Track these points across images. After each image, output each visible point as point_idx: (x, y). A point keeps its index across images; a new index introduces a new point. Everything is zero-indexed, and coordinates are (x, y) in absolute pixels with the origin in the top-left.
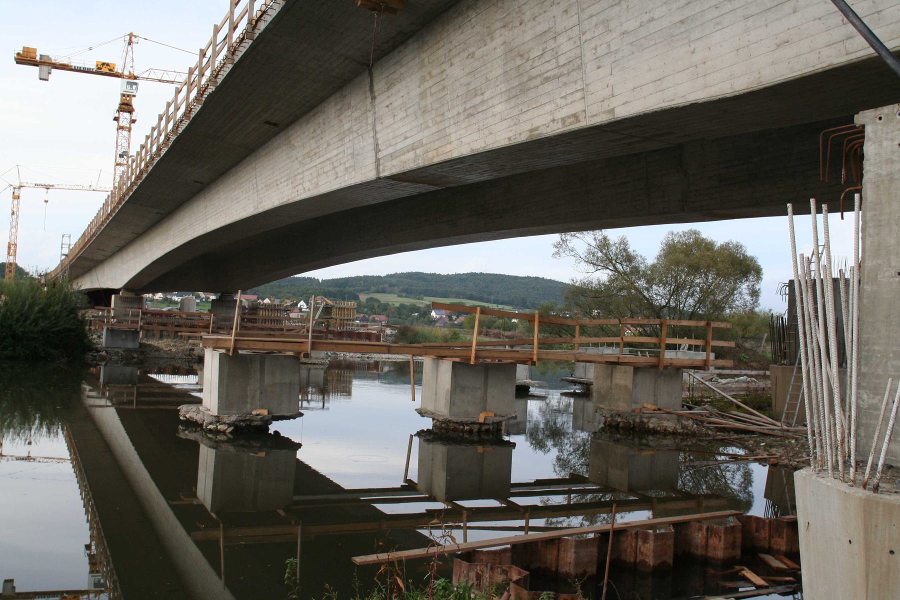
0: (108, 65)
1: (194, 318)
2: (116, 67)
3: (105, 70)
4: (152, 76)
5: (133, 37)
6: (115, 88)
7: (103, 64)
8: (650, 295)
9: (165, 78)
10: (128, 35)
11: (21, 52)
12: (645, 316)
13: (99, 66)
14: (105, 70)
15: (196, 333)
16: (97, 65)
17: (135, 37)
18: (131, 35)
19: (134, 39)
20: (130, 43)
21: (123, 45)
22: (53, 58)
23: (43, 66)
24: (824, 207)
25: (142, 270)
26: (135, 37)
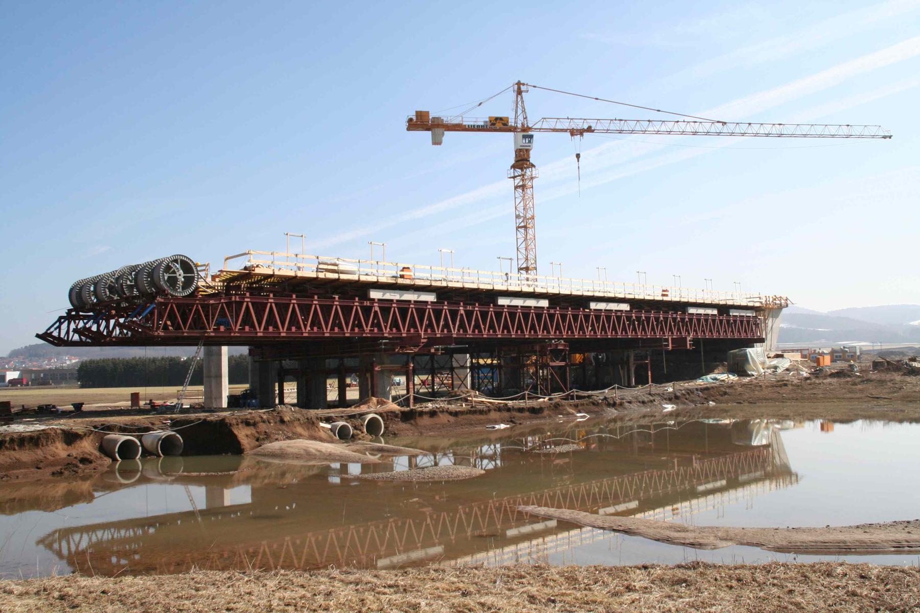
0: (501, 119)
1: (893, 549)
2: (510, 121)
3: (498, 125)
4: (545, 126)
5: (521, 86)
6: (506, 143)
7: (497, 119)
8: (493, 463)
9: (559, 126)
10: (516, 84)
11: (414, 118)
12: (867, 578)
13: (492, 122)
14: (498, 125)
15: (92, 404)
16: (491, 121)
17: (524, 84)
18: (519, 84)
19: (523, 88)
20: (519, 92)
21: (513, 95)
22: (445, 119)
23: (436, 130)
24: (475, 354)
25: (229, 367)
26: (524, 84)
